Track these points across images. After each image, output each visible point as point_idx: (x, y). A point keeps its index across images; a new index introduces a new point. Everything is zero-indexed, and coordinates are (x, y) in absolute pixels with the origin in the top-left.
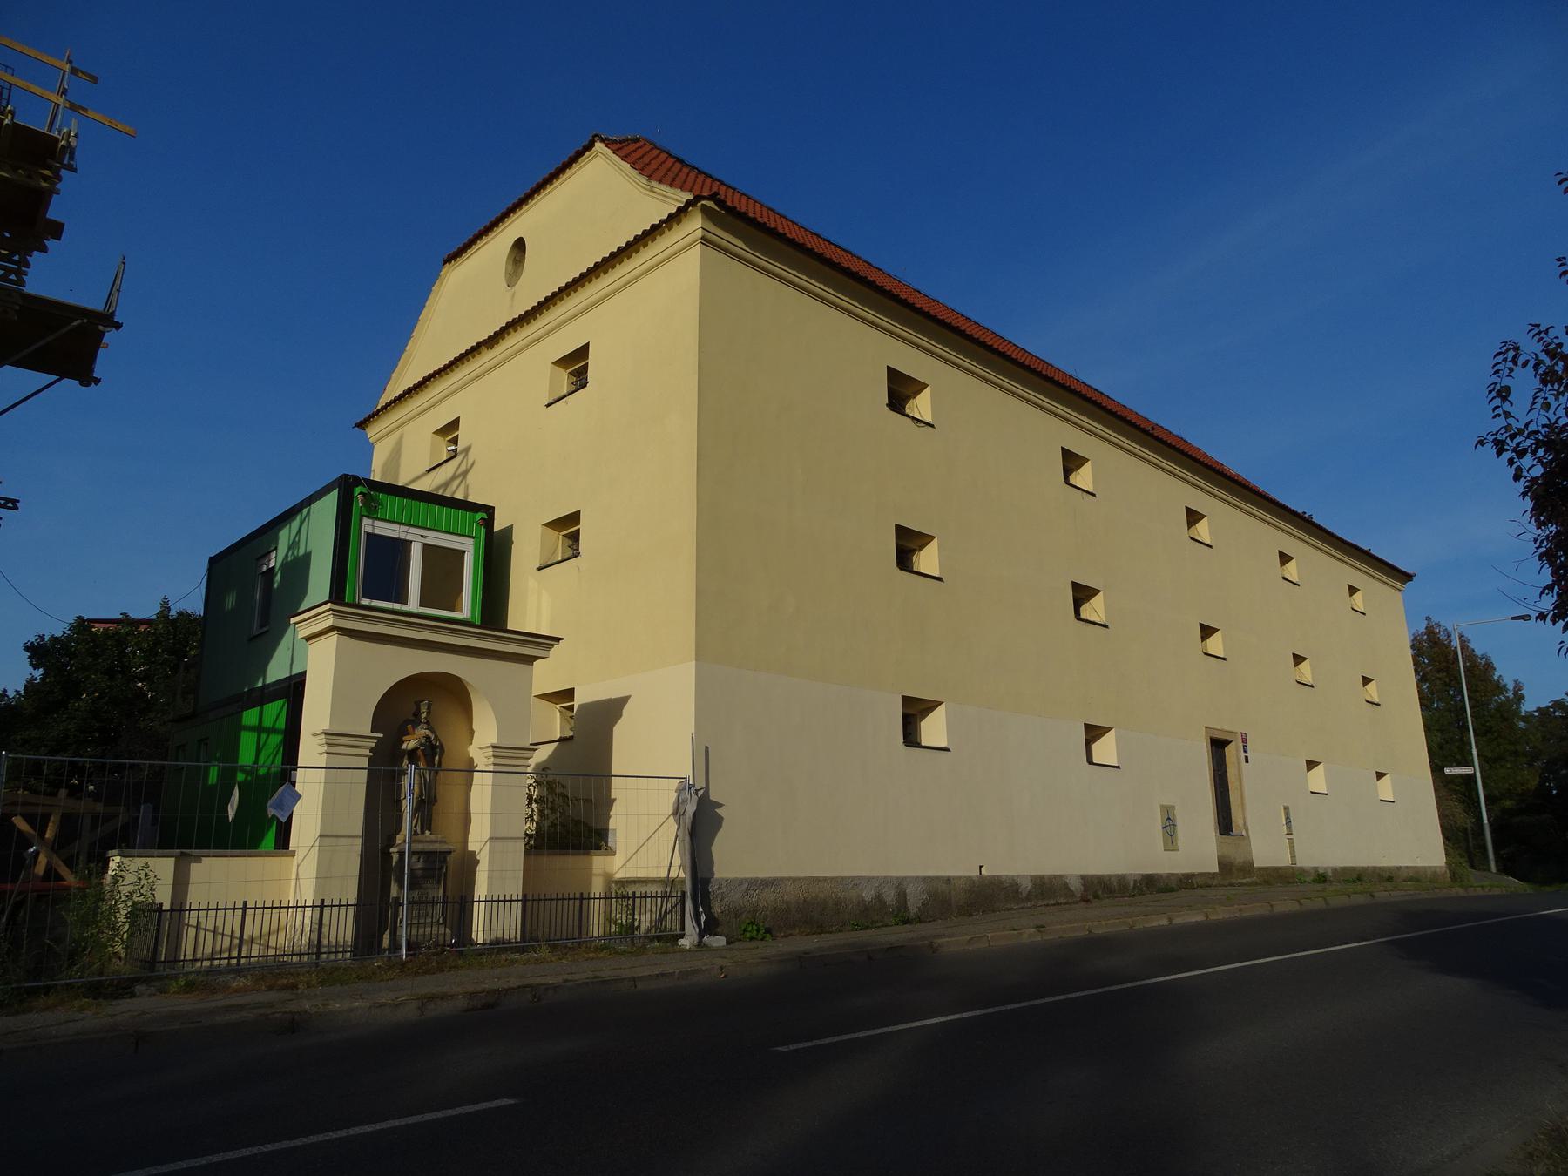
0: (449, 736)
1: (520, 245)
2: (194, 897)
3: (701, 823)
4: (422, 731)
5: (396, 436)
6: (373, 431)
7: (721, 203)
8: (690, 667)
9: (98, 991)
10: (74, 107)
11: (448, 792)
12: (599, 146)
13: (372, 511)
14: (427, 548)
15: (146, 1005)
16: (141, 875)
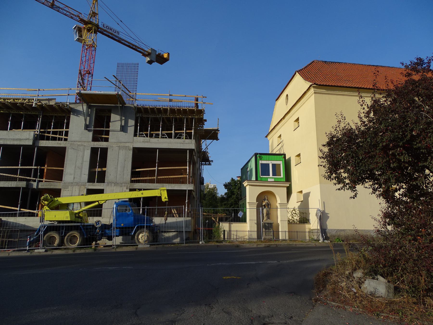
0: (272, 202)
1: (287, 95)
2: (232, 230)
3: (323, 217)
4: (266, 201)
5: (272, 139)
6: (269, 137)
7: (317, 84)
8: (319, 185)
9: (217, 242)
10: (204, 103)
11: (273, 212)
12: (297, 73)
13: (261, 159)
14: (273, 164)
15: (224, 243)
16: (225, 226)
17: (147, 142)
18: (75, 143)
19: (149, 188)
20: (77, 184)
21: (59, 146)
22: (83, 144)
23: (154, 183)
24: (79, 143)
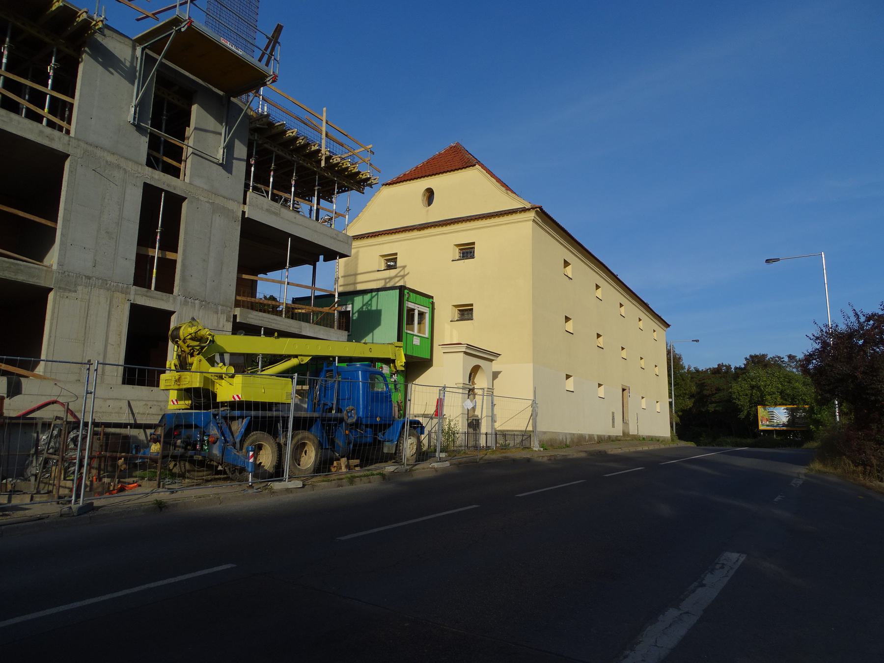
17: (276, 214)
18: (99, 153)
19: (296, 331)
20: (104, 283)
21: (45, 142)
22: (123, 163)
23: (332, 327)
24: (110, 158)
